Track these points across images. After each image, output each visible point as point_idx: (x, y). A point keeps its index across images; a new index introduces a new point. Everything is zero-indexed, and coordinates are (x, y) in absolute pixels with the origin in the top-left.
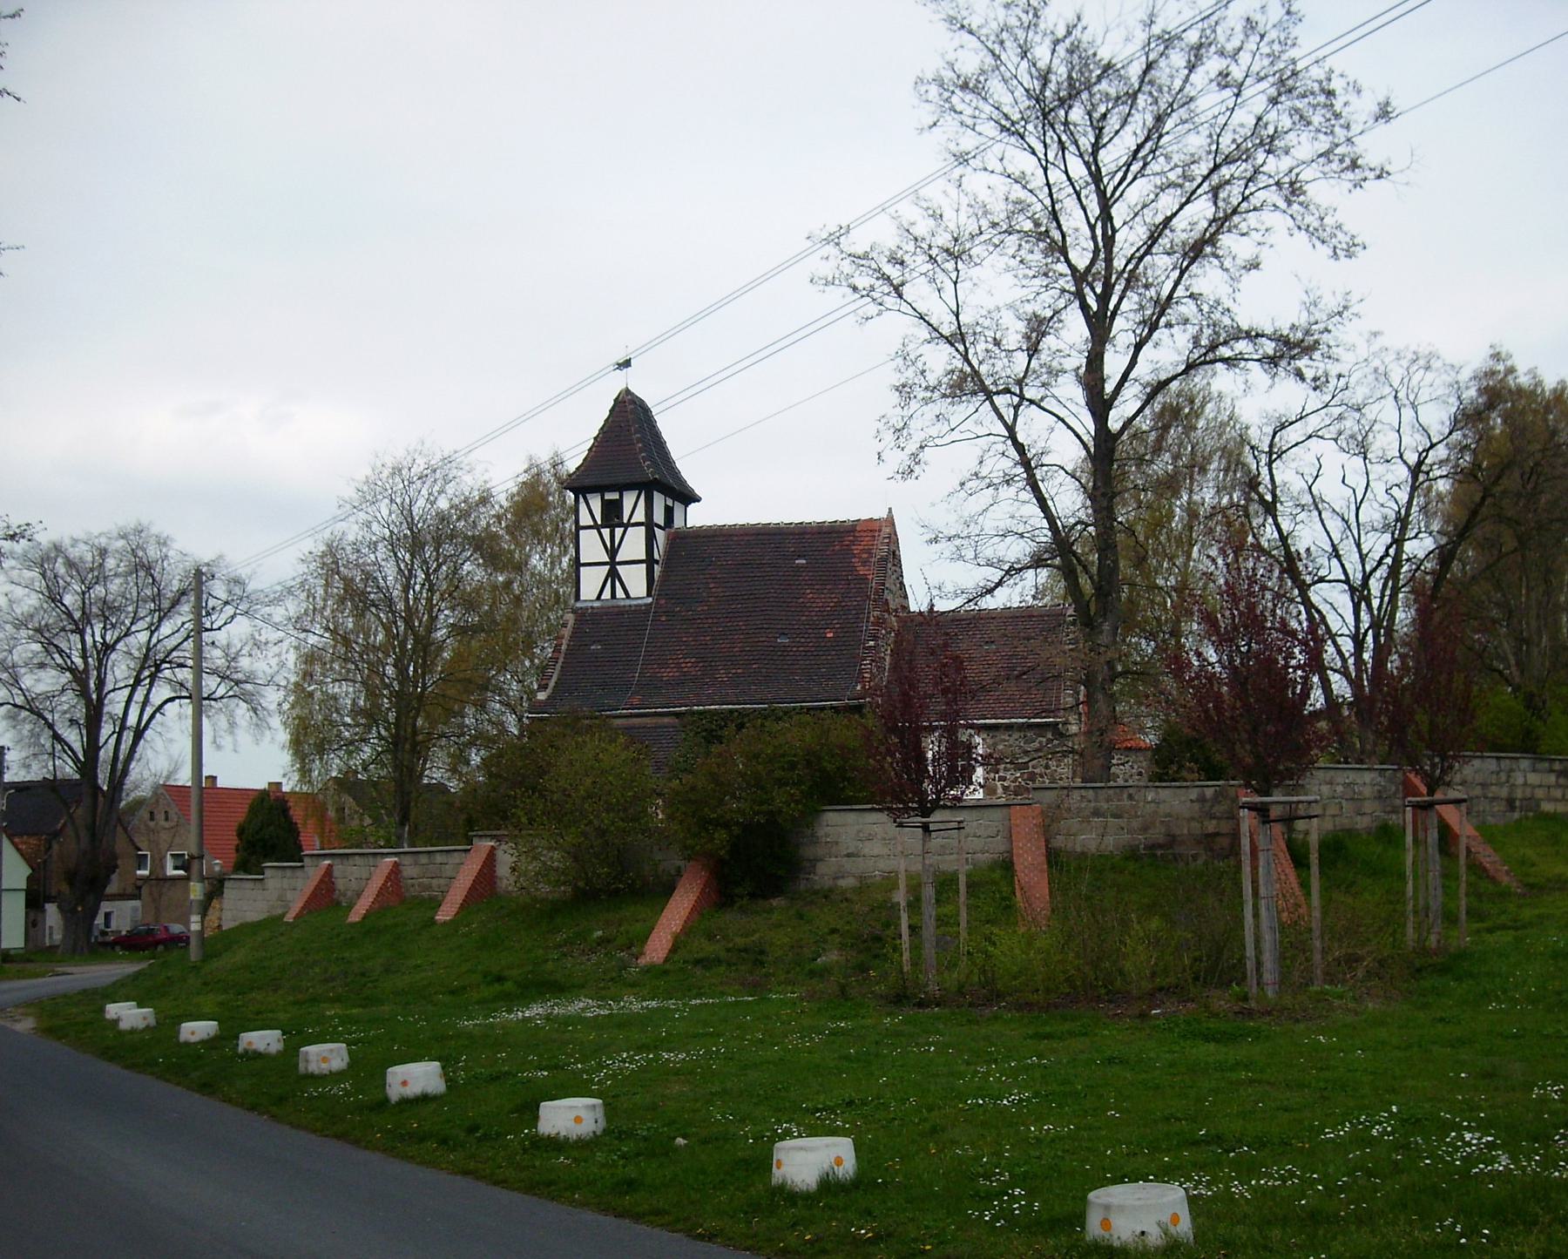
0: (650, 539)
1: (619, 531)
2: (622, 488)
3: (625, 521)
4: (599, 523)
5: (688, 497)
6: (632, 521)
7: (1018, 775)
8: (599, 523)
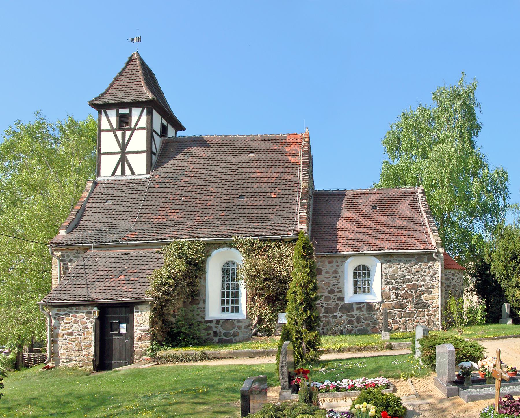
0: (150, 139)
1: (128, 133)
2: (131, 105)
3: (133, 126)
4: (115, 127)
5: (183, 129)
7: (405, 286)
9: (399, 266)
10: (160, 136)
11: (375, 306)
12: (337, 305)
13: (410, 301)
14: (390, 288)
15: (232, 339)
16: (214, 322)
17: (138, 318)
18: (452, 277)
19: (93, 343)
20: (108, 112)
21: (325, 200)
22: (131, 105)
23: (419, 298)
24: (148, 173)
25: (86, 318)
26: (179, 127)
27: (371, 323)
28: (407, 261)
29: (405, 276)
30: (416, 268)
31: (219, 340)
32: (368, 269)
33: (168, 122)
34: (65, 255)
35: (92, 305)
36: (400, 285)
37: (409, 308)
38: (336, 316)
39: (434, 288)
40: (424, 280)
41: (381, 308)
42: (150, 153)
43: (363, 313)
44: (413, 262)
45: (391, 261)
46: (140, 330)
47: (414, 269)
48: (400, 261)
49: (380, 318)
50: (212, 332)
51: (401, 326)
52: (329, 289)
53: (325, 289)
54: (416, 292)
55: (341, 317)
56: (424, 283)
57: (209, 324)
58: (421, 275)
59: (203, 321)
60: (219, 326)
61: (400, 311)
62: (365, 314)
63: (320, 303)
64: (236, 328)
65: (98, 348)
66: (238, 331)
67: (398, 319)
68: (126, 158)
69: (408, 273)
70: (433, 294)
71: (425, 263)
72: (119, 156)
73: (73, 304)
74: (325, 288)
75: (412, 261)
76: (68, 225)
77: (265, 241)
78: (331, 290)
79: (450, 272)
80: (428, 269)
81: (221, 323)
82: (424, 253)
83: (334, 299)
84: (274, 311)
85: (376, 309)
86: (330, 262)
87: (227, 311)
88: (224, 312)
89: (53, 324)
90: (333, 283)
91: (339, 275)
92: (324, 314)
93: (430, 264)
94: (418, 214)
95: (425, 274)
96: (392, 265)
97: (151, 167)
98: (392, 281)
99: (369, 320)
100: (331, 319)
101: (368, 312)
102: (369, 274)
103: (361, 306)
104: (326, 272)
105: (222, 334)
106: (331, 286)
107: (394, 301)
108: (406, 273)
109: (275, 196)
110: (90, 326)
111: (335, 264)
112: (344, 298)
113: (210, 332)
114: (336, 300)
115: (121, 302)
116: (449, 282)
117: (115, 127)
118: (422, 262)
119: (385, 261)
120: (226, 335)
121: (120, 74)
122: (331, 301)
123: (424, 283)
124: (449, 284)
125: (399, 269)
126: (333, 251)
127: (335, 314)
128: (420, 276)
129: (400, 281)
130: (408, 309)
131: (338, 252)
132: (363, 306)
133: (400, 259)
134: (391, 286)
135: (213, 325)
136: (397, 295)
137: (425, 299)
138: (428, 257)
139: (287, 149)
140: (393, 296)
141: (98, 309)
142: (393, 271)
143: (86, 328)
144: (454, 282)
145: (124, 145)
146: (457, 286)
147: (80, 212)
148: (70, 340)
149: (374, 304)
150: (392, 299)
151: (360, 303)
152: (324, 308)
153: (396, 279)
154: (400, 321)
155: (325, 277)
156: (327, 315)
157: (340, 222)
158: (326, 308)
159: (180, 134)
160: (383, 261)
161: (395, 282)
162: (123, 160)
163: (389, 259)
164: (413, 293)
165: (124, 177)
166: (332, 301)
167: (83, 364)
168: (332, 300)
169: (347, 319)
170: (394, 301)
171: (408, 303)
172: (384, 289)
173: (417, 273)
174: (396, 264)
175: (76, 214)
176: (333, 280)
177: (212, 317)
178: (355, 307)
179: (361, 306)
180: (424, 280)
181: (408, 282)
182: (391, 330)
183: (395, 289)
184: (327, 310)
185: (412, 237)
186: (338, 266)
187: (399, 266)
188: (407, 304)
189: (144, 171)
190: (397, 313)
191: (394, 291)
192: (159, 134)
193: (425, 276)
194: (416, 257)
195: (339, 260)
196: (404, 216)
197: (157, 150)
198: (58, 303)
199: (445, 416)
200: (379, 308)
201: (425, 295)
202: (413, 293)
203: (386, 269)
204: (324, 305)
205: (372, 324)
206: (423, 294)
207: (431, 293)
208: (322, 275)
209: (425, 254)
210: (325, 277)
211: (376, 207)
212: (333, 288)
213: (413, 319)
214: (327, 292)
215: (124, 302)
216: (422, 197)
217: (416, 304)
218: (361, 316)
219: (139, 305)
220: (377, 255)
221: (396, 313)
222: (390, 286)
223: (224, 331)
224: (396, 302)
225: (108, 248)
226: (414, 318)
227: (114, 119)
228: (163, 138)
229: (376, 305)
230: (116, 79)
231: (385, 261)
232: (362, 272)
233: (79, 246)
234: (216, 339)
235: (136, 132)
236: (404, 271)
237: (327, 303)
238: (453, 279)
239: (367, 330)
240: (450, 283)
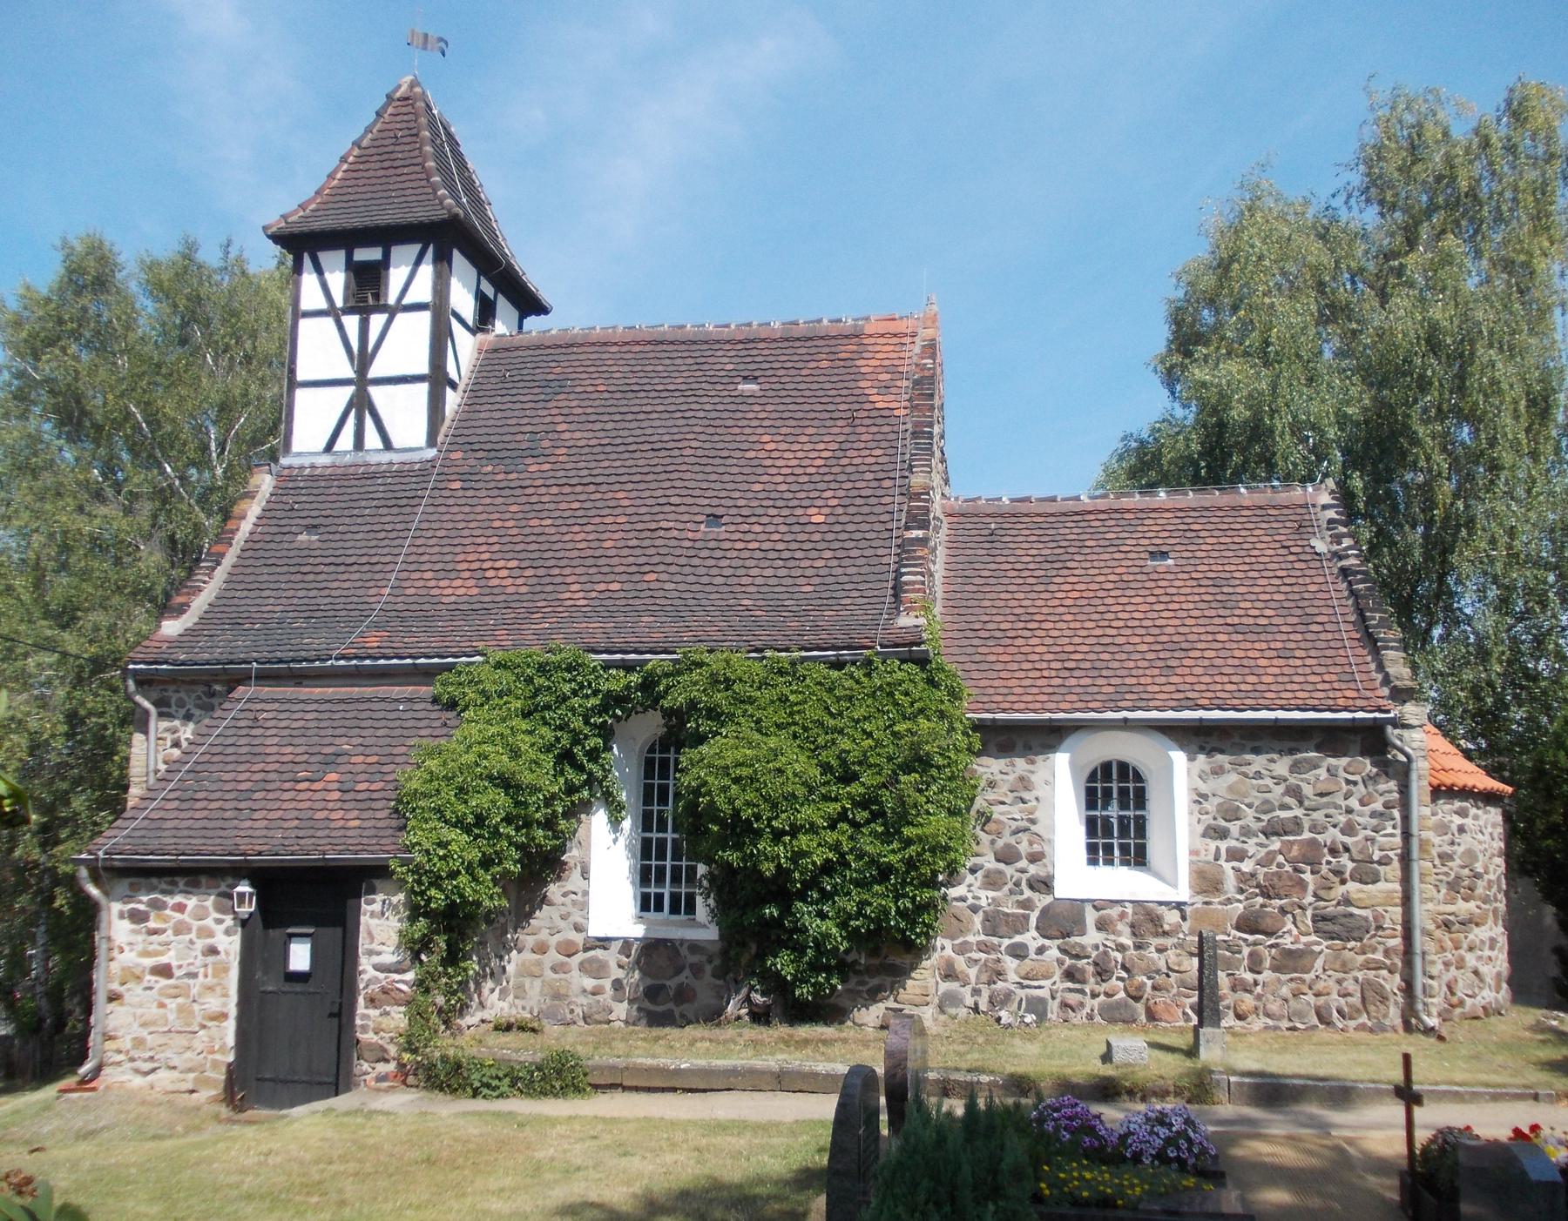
0: (440, 339)
1: (377, 321)
2: (389, 236)
3: (392, 300)
4: (339, 303)
5: (539, 308)
6: (405, 301)
10: (473, 331)
12: (1027, 905)
14: (1218, 849)
16: (616, 946)
17: (374, 922)
18: (1458, 820)
19: (233, 1011)
20: (324, 257)
22: (389, 236)
26: (529, 304)
32: (1138, 777)
33: (499, 289)
34: (173, 701)
35: (238, 871)
38: (1018, 952)
46: (377, 968)
50: (607, 984)
52: (1000, 843)
55: (1041, 950)
57: (599, 953)
59: (579, 938)
63: (970, 895)
64: (687, 972)
68: (369, 396)
72: (349, 391)
87: (659, 908)
88: (648, 910)
90: (1014, 825)
91: (1035, 793)
92: (983, 937)
94: (1321, 580)
102: (1141, 799)
103: (1114, 912)
106: (1007, 832)
109: (821, 519)
117: (339, 303)
123: (1348, 840)
126: (1016, 706)
127: (1018, 939)
129: (1256, 826)
132: (1123, 915)
134: (1223, 845)
139: (865, 366)
141: (252, 885)
142: (1230, 789)
143: (213, 951)
144: (1466, 841)
145: (363, 359)
146: (1481, 856)
148: (162, 992)
152: (981, 913)
156: (995, 940)
159: (533, 323)
162: (361, 404)
163: (1214, 742)
165: (360, 457)
167: (196, 1080)
169: (1060, 962)
178: (1091, 916)
179: (1114, 912)
180: (1349, 830)
185: (1299, 662)
192: (470, 323)
196: (1269, 589)
197: (463, 373)
199: (6, 416)
202: (1308, 877)
204: (983, 902)
209: (1353, 728)
211: (1164, 555)
212: (1012, 841)
216: (1330, 521)
219: (378, 877)
227: (337, 280)
228: (480, 336)
232: (1115, 786)
233: (213, 673)
237: (991, 894)
238: (1461, 829)
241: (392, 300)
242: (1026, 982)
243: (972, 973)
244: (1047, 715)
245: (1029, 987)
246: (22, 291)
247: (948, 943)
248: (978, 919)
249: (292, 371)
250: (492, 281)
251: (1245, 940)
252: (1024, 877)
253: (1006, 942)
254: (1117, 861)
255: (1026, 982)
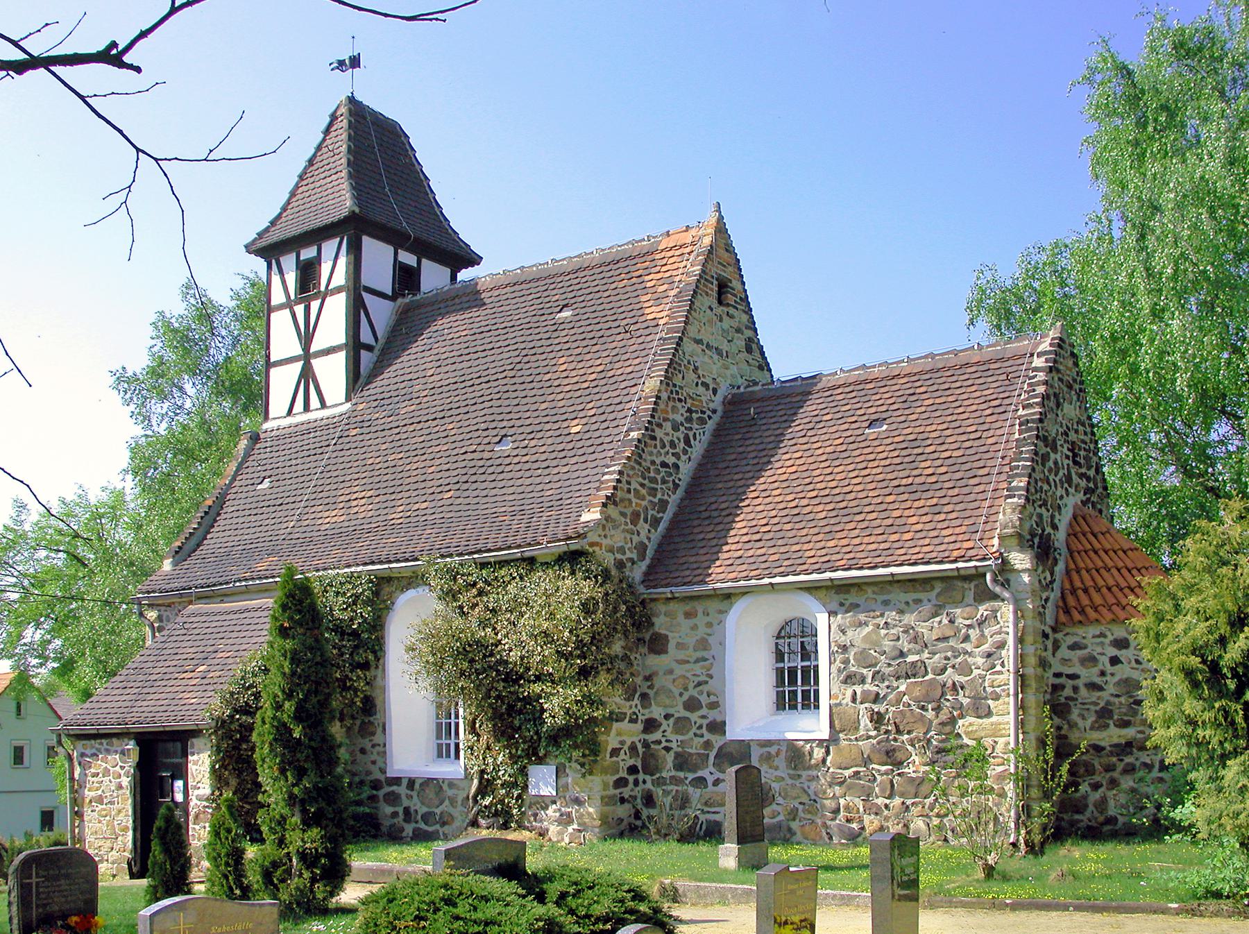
0: (357, 309)
1: (315, 305)
2: (317, 235)
3: (323, 288)
4: (293, 297)
5: (472, 260)
7: (903, 688)
8: (293, 297)
9: (882, 622)
11: (811, 754)
12: (708, 745)
13: (920, 741)
15: (438, 832)
16: (405, 782)
18: (1113, 652)
19: (130, 824)
21: (747, 418)
22: (317, 235)
23: (948, 729)
24: (348, 399)
25: (120, 764)
27: (801, 807)
28: (907, 603)
29: (902, 654)
30: (936, 625)
31: (414, 830)
36: (887, 683)
37: (916, 765)
38: (700, 782)
39: (997, 697)
40: (966, 669)
41: (829, 759)
42: (355, 346)
43: (777, 773)
44: (927, 608)
45: (858, 606)
47: (930, 629)
48: (886, 603)
49: (825, 792)
50: (400, 810)
51: (890, 824)
52: (686, 696)
53: (677, 696)
54: (938, 709)
56: (963, 679)
57: (394, 788)
58: (953, 649)
59: (382, 778)
60: (414, 794)
61: (886, 773)
62: (783, 779)
63: (663, 740)
64: (447, 802)
65: (139, 836)
66: (451, 810)
67: (880, 801)
69: (912, 646)
70: (994, 719)
71: (968, 609)
73: (95, 732)
74: (676, 692)
75: (925, 602)
76: (179, 547)
77: (483, 565)
78: (692, 698)
79: (1102, 635)
80: (977, 629)
81: (417, 786)
82: (974, 571)
83: (700, 727)
84: (514, 758)
85: (813, 762)
86: (688, 615)
89: (76, 776)
90: (697, 679)
91: (712, 652)
92: (673, 773)
93: (983, 610)
95: (968, 647)
96: (862, 617)
97: (356, 380)
98: (864, 671)
99: (795, 798)
100: (691, 789)
101: (792, 772)
103: (773, 750)
104: (680, 646)
105: (419, 817)
107: (869, 737)
108: (905, 645)
110: (126, 781)
111: (701, 620)
112: (724, 723)
113: (397, 809)
114: (704, 730)
115: (162, 729)
116: (1096, 670)
118: (959, 603)
119: (842, 604)
120: (426, 818)
121: (311, 162)
122: (691, 734)
123: (963, 679)
124: (1098, 680)
125: (883, 632)
127: (700, 774)
128: (949, 654)
129: (887, 670)
130: (912, 769)
131: (706, 583)
133: (885, 597)
134: (858, 689)
135: (402, 790)
136: (878, 719)
137: (967, 733)
138: (976, 586)
140: (865, 722)
147: (212, 513)
149: (808, 746)
150: (862, 732)
151: (768, 743)
152: (672, 753)
153: (875, 665)
154: (886, 806)
155: (677, 661)
156: (681, 774)
157: (760, 484)
158: (677, 755)
160: (834, 606)
161: (871, 674)
163: (852, 598)
164: (930, 714)
166: (695, 735)
168: (694, 730)
170: (869, 737)
171: (913, 746)
172: (837, 697)
173: (941, 645)
174: (872, 614)
175: (202, 518)
176: (698, 669)
177: (399, 771)
179: (773, 750)
181: (914, 676)
182: (860, 834)
183: (872, 697)
184: (683, 762)
186: (709, 625)
187: (882, 622)
188: (909, 748)
189: (342, 397)
190: (879, 778)
191: (867, 705)
193: (966, 653)
194: (939, 587)
195: (713, 605)
197: (379, 335)
198: (90, 729)
200: (824, 761)
201: (970, 719)
203: (843, 632)
204: (674, 745)
205: (803, 811)
206: (962, 716)
207: (989, 714)
208: (666, 652)
209: (965, 577)
210: (677, 661)
212: (695, 693)
213: (928, 801)
214: (681, 707)
215: (167, 729)
217: (940, 751)
218: (773, 785)
219: (194, 737)
220: (817, 588)
221: (875, 779)
222: (855, 687)
223: (424, 809)
224: (875, 741)
225: (224, 596)
226: (932, 798)
229: (816, 750)
230: (301, 177)
231: (842, 604)
234: (409, 829)
235: (328, 300)
236: (898, 639)
237: (680, 738)
238: (1115, 661)
239: (790, 829)
240: (1103, 674)
241: (323, 288)
242: (706, 809)
243: (668, 800)
244: (828, 575)
245: (708, 812)
246: (177, 308)
247: (648, 778)
248: (670, 758)
249: (268, 356)
250: (410, 250)
251: (879, 771)
252: (705, 722)
253: (691, 776)
254: (799, 706)
255: (706, 809)
